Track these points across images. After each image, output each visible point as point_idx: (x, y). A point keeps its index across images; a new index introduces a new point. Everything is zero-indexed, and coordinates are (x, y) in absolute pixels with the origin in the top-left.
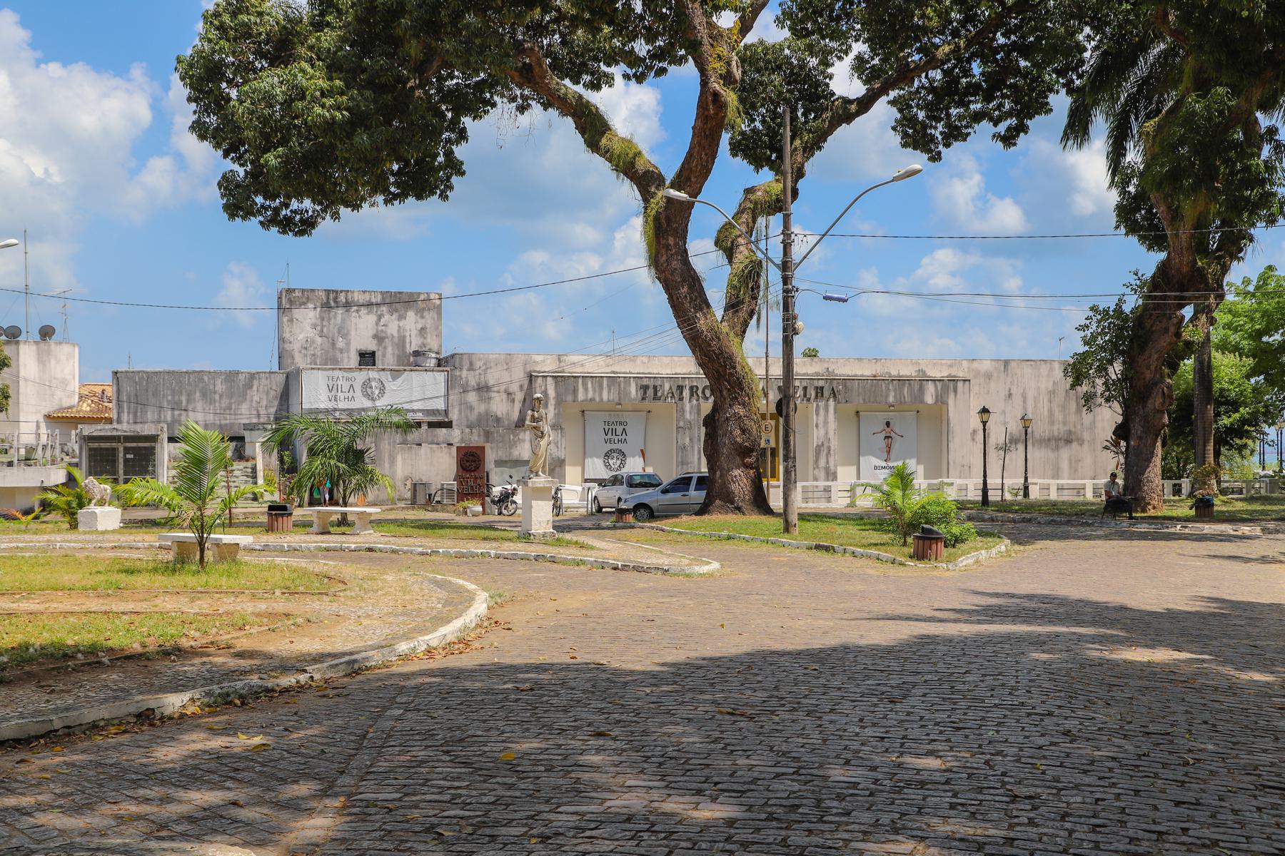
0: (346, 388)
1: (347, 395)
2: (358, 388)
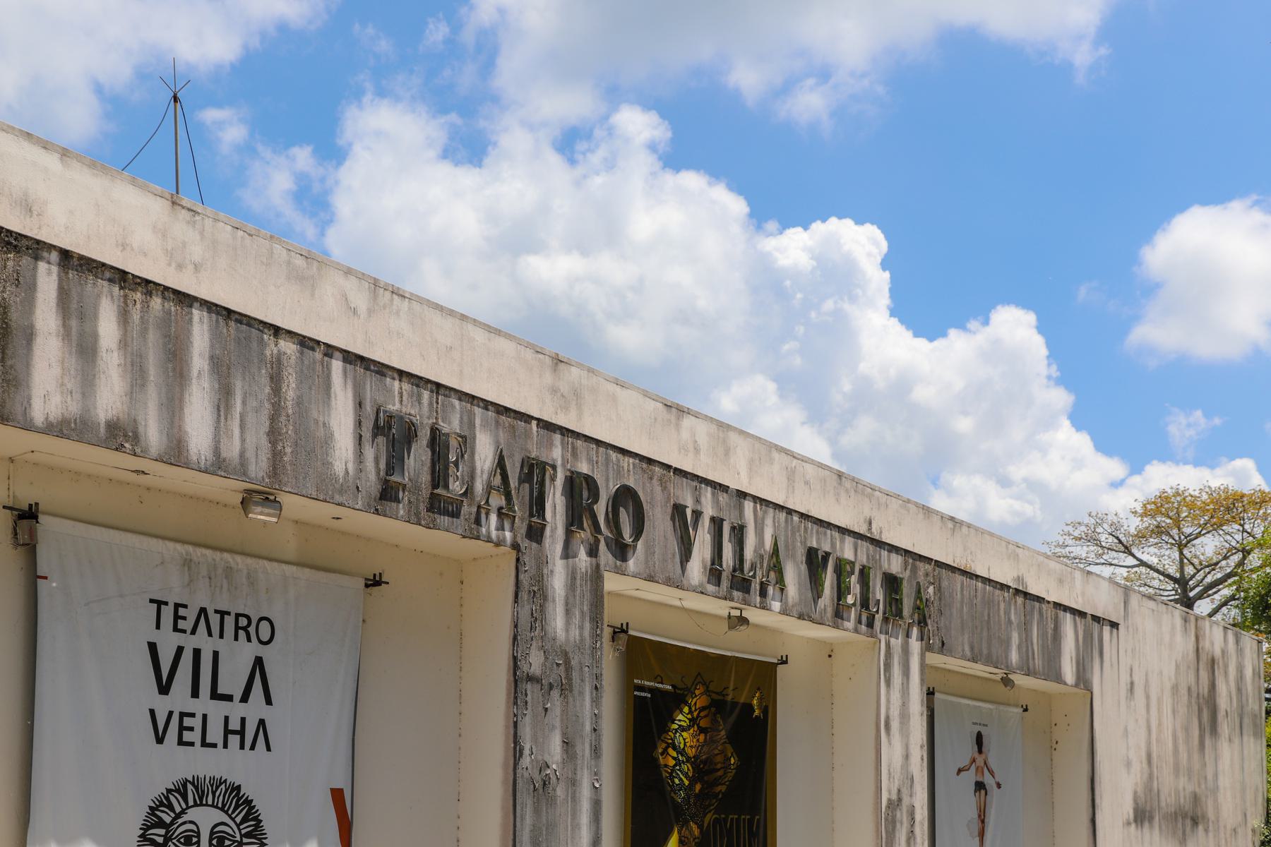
0: (232, 682)
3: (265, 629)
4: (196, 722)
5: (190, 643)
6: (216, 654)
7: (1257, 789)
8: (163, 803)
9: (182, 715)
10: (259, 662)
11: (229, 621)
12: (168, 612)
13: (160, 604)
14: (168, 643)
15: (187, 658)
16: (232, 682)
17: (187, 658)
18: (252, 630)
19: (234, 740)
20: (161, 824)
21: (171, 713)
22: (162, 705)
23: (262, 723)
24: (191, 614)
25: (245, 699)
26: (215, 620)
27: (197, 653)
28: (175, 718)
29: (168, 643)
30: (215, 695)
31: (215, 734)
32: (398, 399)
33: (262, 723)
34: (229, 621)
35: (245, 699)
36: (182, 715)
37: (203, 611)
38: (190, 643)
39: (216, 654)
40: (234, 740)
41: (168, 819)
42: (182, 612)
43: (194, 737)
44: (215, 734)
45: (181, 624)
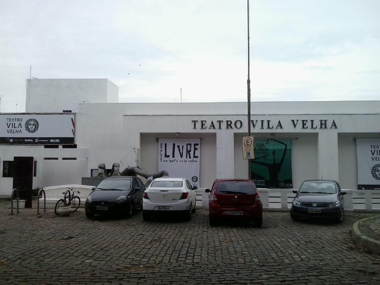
1: (17, 129)
2: (23, 124)
3: (21, 120)
4: (12, 131)
5: (376, 150)
6: (15, 123)
7: (35, 176)
8: (374, 167)
9: (376, 157)
10: (20, 124)
11: (16, 120)
12: (9, 120)
13: (372, 146)
14: (9, 123)
15: (11, 124)
16: (17, 126)
17: (11, 124)
18: (19, 120)
19: (17, 132)
20: (374, 169)
21: (374, 157)
22: (8, 129)
23: (20, 130)
24: (376, 146)
25: (18, 128)
26: (14, 120)
27: (12, 123)
28: (10, 130)
29: (9, 123)
30: (15, 128)
31: (15, 132)
32: (195, 119)
33: (20, 130)
34: (16, 120)
35: (18, 128)
36: (376, 157)
37: (378, 146)
38: (11, 122)
39: (15, 123)
40: (17, 132)
41: (28, 123)
42: (375, 146)
43: (12, 132)
44: (15, 132)
45: (10, 121)
